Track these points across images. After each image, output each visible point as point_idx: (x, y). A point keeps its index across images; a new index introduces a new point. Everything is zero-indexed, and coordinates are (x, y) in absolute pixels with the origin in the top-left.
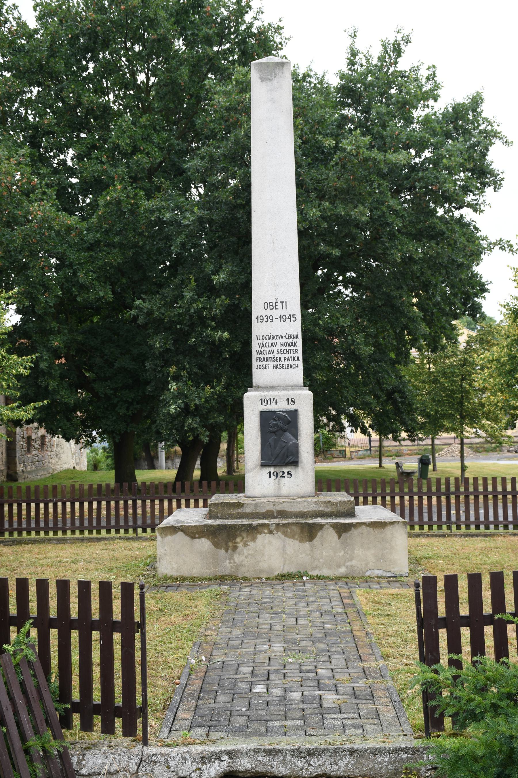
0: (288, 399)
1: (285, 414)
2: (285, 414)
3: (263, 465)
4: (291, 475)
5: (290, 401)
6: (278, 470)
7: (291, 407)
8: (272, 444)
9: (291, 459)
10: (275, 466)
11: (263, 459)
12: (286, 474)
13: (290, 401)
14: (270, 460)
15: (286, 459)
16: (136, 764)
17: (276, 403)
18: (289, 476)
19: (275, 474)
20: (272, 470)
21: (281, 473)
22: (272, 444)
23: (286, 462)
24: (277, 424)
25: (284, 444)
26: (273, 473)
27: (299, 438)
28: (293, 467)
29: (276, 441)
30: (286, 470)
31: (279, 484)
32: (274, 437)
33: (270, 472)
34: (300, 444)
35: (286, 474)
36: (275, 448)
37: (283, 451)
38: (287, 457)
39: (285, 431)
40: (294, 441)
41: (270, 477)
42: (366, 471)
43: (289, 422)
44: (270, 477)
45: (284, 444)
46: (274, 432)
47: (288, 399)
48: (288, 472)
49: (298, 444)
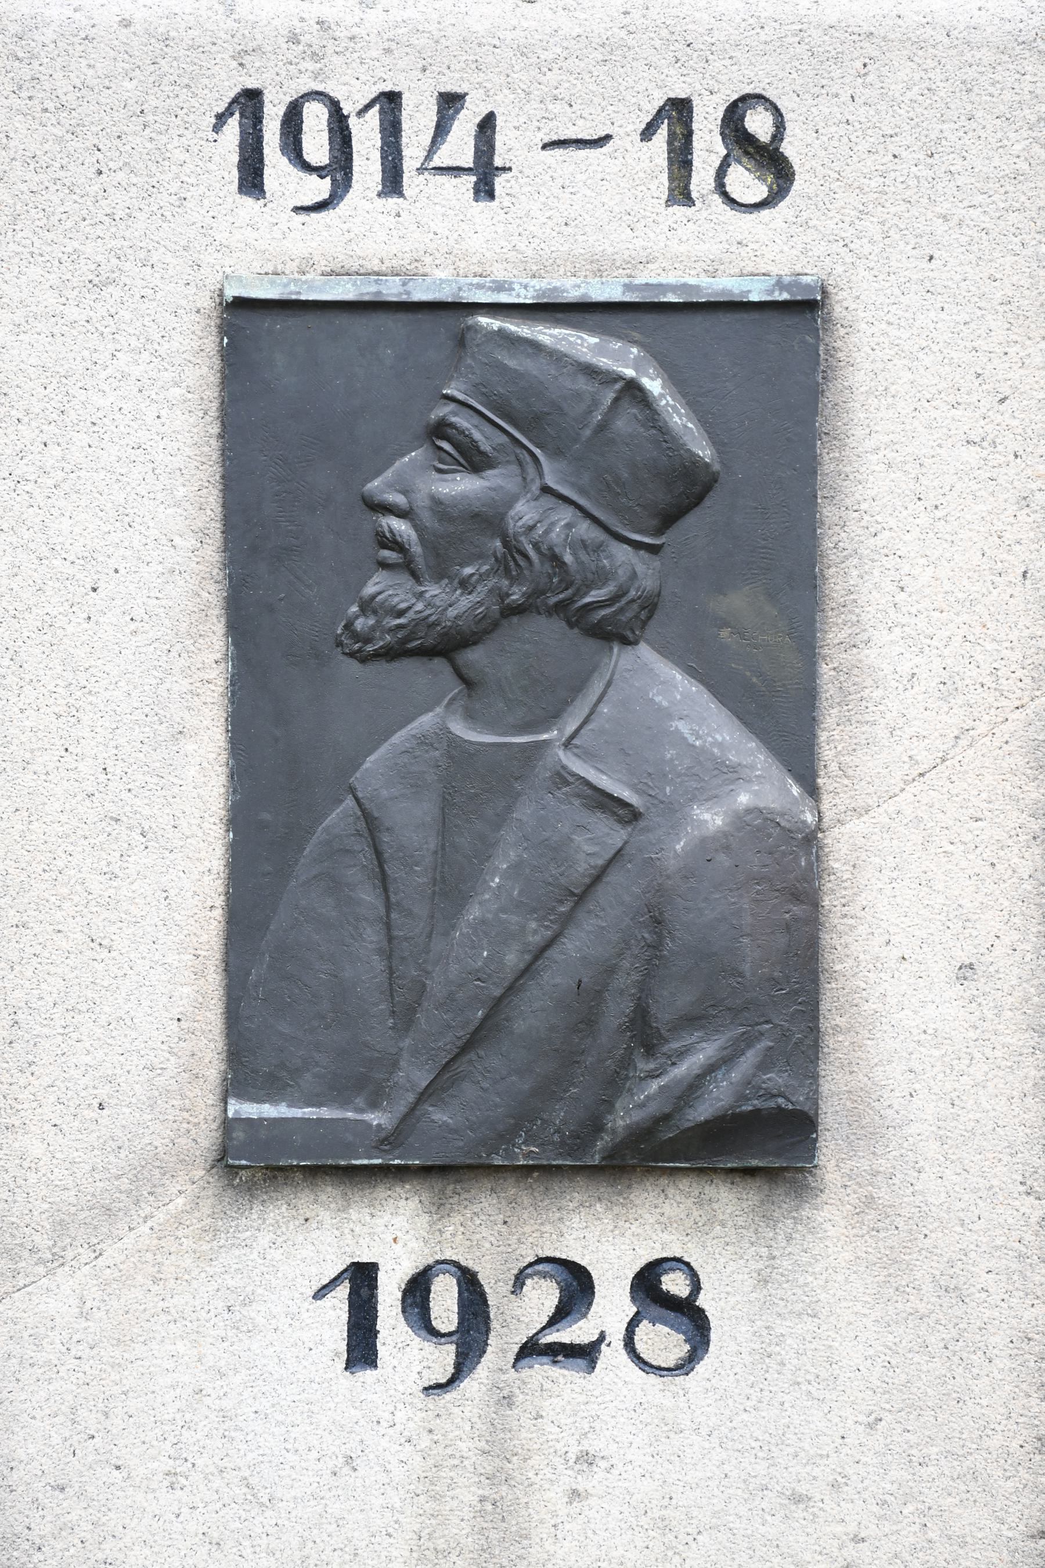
0: (678, 111)
1: (621, 357)
2: (621, 357)
3: (254, 1165)
4: (691, 1318)
5: (708, 145)
6: (490, 1234)
7: (723, 248)
8: (412, 822)
9: (704, 1070)
10: (445, 1174)
11: (246, 1066)
12: (612, 1307)
13: (708, 145)
14: (363, 1083)
15: (616, 1083)
16: (380, 951)
17: (485, 176)
18: (661, 1341)
19: (445, 1302)
20: (396, 1232)
21: (543, 1296)
22: (412, 822)
23: (623, 1118)
24: (487, 519)
25: (597, 838)
26: (417, 1291)
27: (833, 741)
28: (728, 1200)
29: (474, 789)
30: (613, 1236)
31: (501, 1460)
32: (437, 718)
33: (362, 1277)
34: (841, 845)
35: (612, 1307)
36: (452, 888)
37: (576, 945)
38: (645, 1036)
39: (612, 631)
40: (762, 786)
41: (362, 1349)
42: (464, 497)
43: (682, 492)
44: (362, 1349)
45: (597, 838)
46: (445, 646)
47: (678, 111)
48: (647, 1283)
49: (810, 840)
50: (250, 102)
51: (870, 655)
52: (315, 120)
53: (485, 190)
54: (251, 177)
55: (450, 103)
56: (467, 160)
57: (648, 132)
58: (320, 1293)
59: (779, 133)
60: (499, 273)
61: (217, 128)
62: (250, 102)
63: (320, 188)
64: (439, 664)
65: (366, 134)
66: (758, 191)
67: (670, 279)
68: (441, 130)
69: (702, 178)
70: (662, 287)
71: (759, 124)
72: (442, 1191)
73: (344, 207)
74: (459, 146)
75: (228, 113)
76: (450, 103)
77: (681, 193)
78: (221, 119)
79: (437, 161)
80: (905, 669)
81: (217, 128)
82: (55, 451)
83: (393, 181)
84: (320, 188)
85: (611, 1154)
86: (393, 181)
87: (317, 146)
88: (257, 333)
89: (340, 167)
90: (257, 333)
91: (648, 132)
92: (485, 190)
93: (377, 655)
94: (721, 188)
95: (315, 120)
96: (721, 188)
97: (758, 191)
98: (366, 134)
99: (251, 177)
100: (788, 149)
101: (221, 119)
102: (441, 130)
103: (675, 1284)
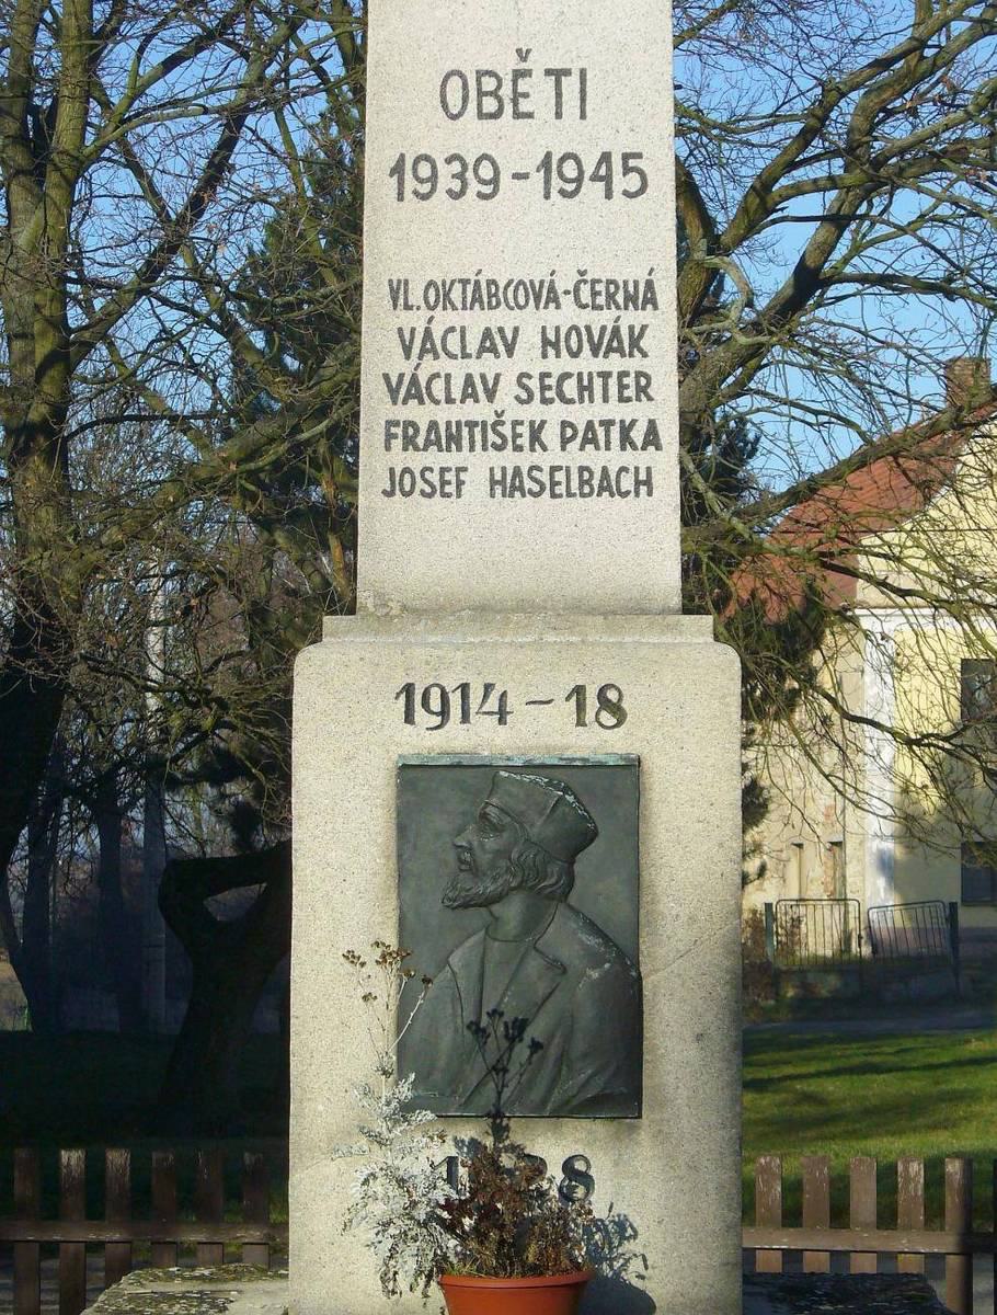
0: (579, 691)
5: (592, 703)
7: (598, 742)
13: (592, 703)
17: (502, 715)
28: (599, 1128)
47: (579, 691)
48: (568, 1166)
50: (408, 689)
51: (661, 907)
52: (435, 694)
53: (502, 721)
54: (409, 718)
55: (488, 688)
56: (496, 710)
57: (568, 699)
58: (516, 330)
59: (620, 699)
60: (508, 753)
61: (396, 698)
62: (408, 689)
63: (437, 720)
64: (483, 910)
65: (455, 700)
66: (613, 721)
67: (578, 755)
68: (486, 696)
69: (590, 715)
70: (574, 759)
71: (612, 695)
72: (406, 1109)
73: (447, 727)
74: (493, 704)
75: (401, 692)
76: (488, 688)
77: (580, 722)
78: (398, 695)
79: (484, 709)
80: (674, 913)
81: (396, 698)
82: (330, 826)
83: (465, 718)
84: (437, 720)
85: (554, 1111)
86: (465, 718)
87: (435, 705)
88: (413, 778)
89: (444, 713)
90: (413, 778)
91: (568, 699)
92: (502, 721)
93: (459, 906)
94: (597, 720)
95: (435, 694)
96: (597, 720)
97: (613, 721)
98: (455, 700)
99: (409, 718)
100: (624, 705)
101: (398, 695)
102: (486, 696)
103: (580, 1166)
